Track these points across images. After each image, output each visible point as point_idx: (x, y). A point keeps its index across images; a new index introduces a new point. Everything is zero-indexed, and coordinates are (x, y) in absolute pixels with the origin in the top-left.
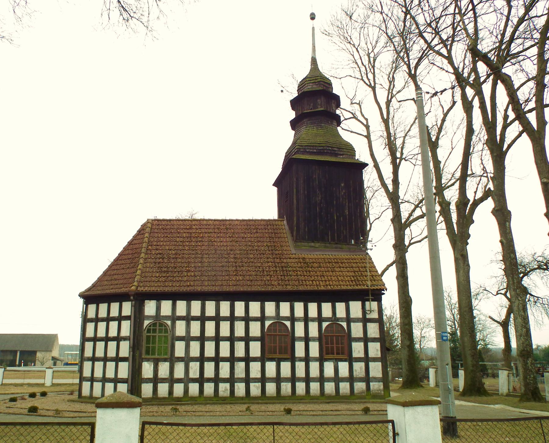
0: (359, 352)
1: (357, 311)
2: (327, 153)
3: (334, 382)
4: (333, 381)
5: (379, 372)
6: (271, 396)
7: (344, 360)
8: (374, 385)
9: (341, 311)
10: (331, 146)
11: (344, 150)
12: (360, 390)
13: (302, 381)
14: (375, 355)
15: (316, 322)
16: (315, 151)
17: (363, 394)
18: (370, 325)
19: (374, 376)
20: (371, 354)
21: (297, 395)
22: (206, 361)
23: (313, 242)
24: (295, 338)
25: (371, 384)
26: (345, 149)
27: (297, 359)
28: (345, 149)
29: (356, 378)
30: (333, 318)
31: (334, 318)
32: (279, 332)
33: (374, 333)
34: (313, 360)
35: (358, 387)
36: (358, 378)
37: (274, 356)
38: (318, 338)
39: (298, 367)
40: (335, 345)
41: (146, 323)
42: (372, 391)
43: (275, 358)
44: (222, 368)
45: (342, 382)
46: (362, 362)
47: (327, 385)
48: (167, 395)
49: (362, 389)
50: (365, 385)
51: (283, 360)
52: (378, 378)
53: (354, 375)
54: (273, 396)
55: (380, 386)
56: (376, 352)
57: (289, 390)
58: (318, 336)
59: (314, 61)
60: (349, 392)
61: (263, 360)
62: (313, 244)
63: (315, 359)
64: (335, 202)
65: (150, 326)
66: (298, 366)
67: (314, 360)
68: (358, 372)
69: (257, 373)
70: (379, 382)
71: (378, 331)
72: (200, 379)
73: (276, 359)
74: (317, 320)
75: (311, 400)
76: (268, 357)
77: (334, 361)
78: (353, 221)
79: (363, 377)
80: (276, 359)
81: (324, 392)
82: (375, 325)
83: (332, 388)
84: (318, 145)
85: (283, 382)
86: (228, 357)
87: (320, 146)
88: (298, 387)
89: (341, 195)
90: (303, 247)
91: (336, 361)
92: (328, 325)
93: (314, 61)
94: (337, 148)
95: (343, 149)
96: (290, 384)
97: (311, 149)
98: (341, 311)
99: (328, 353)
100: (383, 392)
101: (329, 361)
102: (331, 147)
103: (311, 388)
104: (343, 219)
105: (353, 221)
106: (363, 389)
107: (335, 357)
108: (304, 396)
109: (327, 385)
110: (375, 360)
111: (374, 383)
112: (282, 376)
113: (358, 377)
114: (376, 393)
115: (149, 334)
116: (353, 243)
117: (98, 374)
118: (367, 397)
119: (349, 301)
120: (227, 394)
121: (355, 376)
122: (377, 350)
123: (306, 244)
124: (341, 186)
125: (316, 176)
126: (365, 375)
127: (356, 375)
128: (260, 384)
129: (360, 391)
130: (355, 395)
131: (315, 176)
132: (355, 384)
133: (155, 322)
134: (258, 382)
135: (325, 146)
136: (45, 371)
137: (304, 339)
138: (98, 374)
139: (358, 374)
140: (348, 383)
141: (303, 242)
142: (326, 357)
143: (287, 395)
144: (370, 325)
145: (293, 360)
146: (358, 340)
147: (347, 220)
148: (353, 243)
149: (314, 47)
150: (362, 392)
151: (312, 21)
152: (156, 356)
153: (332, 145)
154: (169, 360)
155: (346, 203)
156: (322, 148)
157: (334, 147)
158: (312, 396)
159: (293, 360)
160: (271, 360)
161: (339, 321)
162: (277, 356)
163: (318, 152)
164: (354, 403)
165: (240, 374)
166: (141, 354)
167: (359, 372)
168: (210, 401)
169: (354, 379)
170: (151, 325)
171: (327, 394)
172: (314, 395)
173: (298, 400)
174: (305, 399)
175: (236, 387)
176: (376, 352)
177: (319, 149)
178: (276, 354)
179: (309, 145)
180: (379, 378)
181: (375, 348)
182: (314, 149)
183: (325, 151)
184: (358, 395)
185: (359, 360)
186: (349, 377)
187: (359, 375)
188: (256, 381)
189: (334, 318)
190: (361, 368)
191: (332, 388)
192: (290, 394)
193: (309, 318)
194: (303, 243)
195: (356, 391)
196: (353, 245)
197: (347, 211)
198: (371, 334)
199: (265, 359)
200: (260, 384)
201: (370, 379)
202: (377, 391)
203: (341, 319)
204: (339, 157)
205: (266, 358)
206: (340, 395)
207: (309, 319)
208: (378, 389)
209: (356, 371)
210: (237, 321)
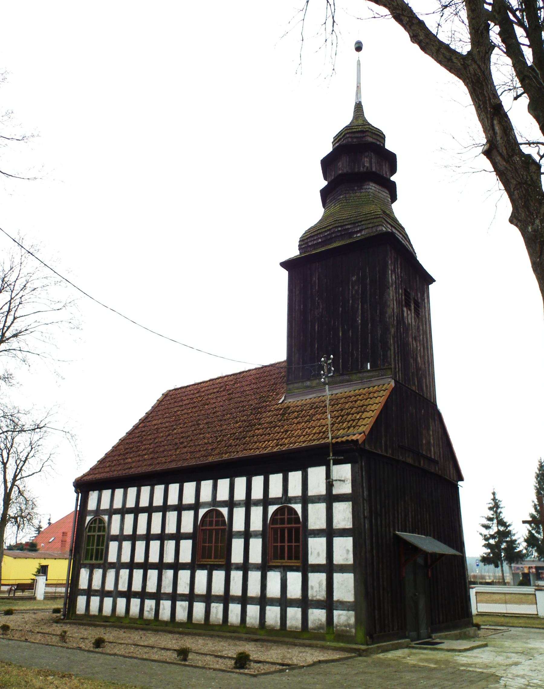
0: (318, 554)
1: (319, 484)
2: (335, 237)
3: (280, 605)
4: (278, 604)
5: (350, 591)
6: (198, 623)
7: (295, 568)
8: (339, 615)
9: (295, 486)
10: (340, 224)
11: (363, 223)
12: (317, 623)
13: (237, 602)
14: (343, 560)
15: (260, 506)
16: (320, 240)
17: (322, 631)
18: (338, 506)
19: (341, 600)
20: (338, 559)
21: (229, 624)
22: (135, 569)
23: (309, 379)
24: (233, 533)
25: (336, 613)
26: (363, 221)
27: (233, 567)
28: (363, 221)
29: (312, 601)
30: (284, 498)
31: (286, 498)
32: (215, 526)
33: (344, 520)
34: (253, 568)
35: (315, 618)
36: (315, 601)
37: (204, 562)
38: (261, 532)
39: (234, 580)
40: (286, 544)
41: (88, 518)
42: (337, 626)
43: (207, 565)
44: (150, 579)
45: (291, 606)
46: (323, 572)
47: (269, 610)
48: (97, 614)
49: (320, 622)
50: (325, 615)
51: (216, 568)
52: (346, 602)
53: (309, 595)
54: (200, 623)
55: (349, 618)
56: (345, 556)
57: (220, 616)
58: (261, 529)
59: (359, 107)
60: (300, 626)
61: (192, 567)
62: (308, 383)
63: (256, 567)
64: (341, 309)
65: (92, 524)
66: (234, 577)
67: (255, 568)
68: (315, 590)
69: (185, 587)
70: (348, 610)
71: (350, 516)
72: (127, 593)
73: (208, 566)
74: (262, 504)
75: (247, 634)
76: (199, 563)
77: (282, 569)
78: (369, 331)
79: (322, 599)
80: (208, 566)
81: (265, 622)
82: (346, 506)
83: (276, 617)
84: (323, 230)
85: (213, 602)
86: (156, 563)
87: (326, 231)
88: (232, 611)
89: (350, 295)
90: (296, 391)
91: (285, 570)
92: (296, 513)
93: (359, 107)
94: (351, 224)
95: (361, 221)
96: (222, 605)
97: (314, 240)
98: (295, 486)
99: (275, 558)
100: (353, 630)
101: (274, 571)
102: (341, 226)
103: (248, 614)
104: (352, 333)
105: (369, 331)
106: (321, 620)
107: (284, 564)
108: (237, 627)
109: (269, 610)
110: (343, 569)
111: (341, 612)
112: (213, 593)
113: (315, 599)
114: (342, 630)
115: (89, 534)
116: (369, 368)
117: (183, 588)
118: (328, 637)
119: (307, 468)
120: (152, 616)
121: (310, 598)
122: (348, 551)
123: (300, 384)
124: (352, 280)
125: (316, 278)
126: (325, 597)
127: (313, 596)
128: (187, 603)
129: (316, 624)
130: (308, 632)
131: (315, 279)
132: (310, 611)
133: (95, 518)
134: (185, 601)
135: (332, 228)
136: (535, 595)
137: (243, 534)
138: (183, 588)
139: (315, 594)
140: (300, 609)
141: (296, 383)
142: (271, 564)
143: (216, 624)
144: (338, 506)
145: (228, 567)
146: (318, 534)
147: (360, 333)
148: (369, 368)
149: (358, 87)
150: (320, 627)
151: (357, 52)
152: (94, 562)
153: (343, 222)
154: (102, 566)
155: (358, 306)
156: (328, 233)
157: (346, 225)
158: (249, 627)
159: (228, 567)
160: (202, 567)
161: (293, 502)
162: (212, 561)
163: (324, 240)
164: (293, 645)
165: (167, 587)
166: (80, 558)
167: (316, 591)
168: (134, 624)
169: (309, 602)
170: (92, 522)
171: (269, 626)
172: (250, 626)
173: (229, 632)
174: (238, 632)
175: (161, 607)
176: (345, 556)
177: (325, 236)
178: (211, 558)
179: (312, 234)
180: (349, 602)
181: (345, 547)
182: (318, 238)
183: (333, 235)
184: (313, 631)
185: (317, 568)
186: (301, 598)
187: (316, 596)
188: (184, 598)
189: (286, 498)
190: (320, 584)
191: (276, 617)
192: (221, 621)
193: (252, 501)
194: (296, 385)
195: (310, 625)
196: (369, 371)
197: (360, 317)
198: (339, 523)
199: (196, 566)
200: (187, 603)
201: (333, 604)
202: (344, 628)
203: (294, 500)
204: (355, 236)
205: (197, 564)
206: (287, 629)
207: (252, 502)
208: (346, 623)
209: (312, 588)
210: (169, 511)
